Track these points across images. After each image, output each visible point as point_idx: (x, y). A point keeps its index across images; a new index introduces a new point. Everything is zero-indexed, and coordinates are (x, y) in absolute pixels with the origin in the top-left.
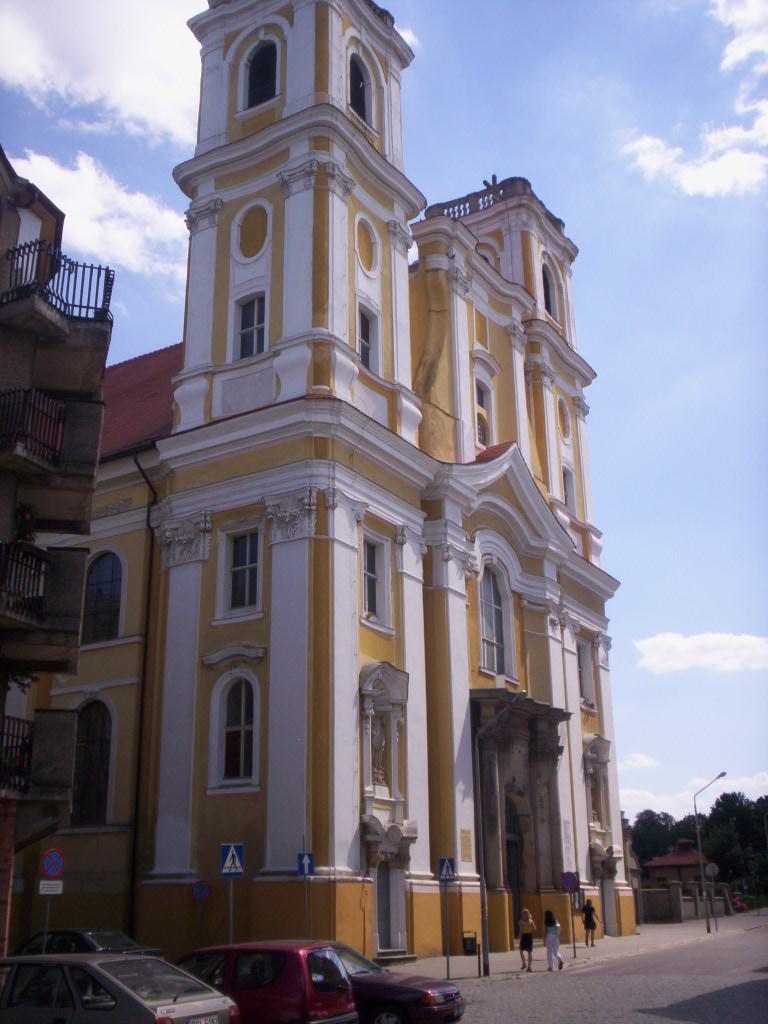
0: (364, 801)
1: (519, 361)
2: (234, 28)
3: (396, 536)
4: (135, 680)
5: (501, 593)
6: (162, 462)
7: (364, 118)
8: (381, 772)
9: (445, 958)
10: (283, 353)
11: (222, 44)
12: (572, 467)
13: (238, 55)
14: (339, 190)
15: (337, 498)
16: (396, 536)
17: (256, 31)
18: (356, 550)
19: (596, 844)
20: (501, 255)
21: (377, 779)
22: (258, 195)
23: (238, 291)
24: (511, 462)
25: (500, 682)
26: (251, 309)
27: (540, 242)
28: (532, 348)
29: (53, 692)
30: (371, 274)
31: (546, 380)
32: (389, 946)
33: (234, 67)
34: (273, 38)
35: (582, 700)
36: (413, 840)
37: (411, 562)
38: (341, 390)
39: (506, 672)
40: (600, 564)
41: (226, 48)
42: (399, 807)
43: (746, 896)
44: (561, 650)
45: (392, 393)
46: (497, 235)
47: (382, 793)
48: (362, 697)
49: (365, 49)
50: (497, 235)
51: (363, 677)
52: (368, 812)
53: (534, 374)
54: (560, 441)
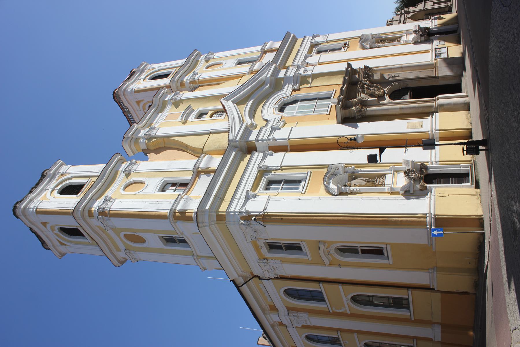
0: (407, 43)
1: (186, 94)
2: (58, 244)
3: (263, 171)
4: (340, 287)
5: (292, 100)
6: (239, 276)
7: (84, 185)
8: (378, 180)
9: (480, 152)
10: (181, 232)
11: (64, 246)
12: (235, 60)
13: (68, 241)
14: (110, 204)
15: (243, 210)
16: (263, 171)
17: (56, 234)
18: (269, 197)
19: (412, 40)
20: (146, 101)
21: (382, 182)
22: (119, 236)
23: (161, 245)
24: (230, 102)
25: (334, 99)
26: (169, 240)
27: (139, 83)
28: (182, 86)
29: (349, 313)
30: (224, 64)
31: (196, 77)
32: (469, 173)
33: (71, 242)
34: (56, 228)
35: (343, 49)
36: (419, 26)
37: (275, 160)
38: (193, 207)
39: (330, 96)
40: (197, 197)
41: (65, 245)
42: (408, 33)
43: (433, 216)
44: (318, 66)
45: (198, 173)
46: (138, 102)
47: (403, 39)
48: (371, 48)
49: (147, 77)
50: (138, 102)
51: (363, 48)
52: (411, 42)
53: (196, 85)
54: (225, 66)
